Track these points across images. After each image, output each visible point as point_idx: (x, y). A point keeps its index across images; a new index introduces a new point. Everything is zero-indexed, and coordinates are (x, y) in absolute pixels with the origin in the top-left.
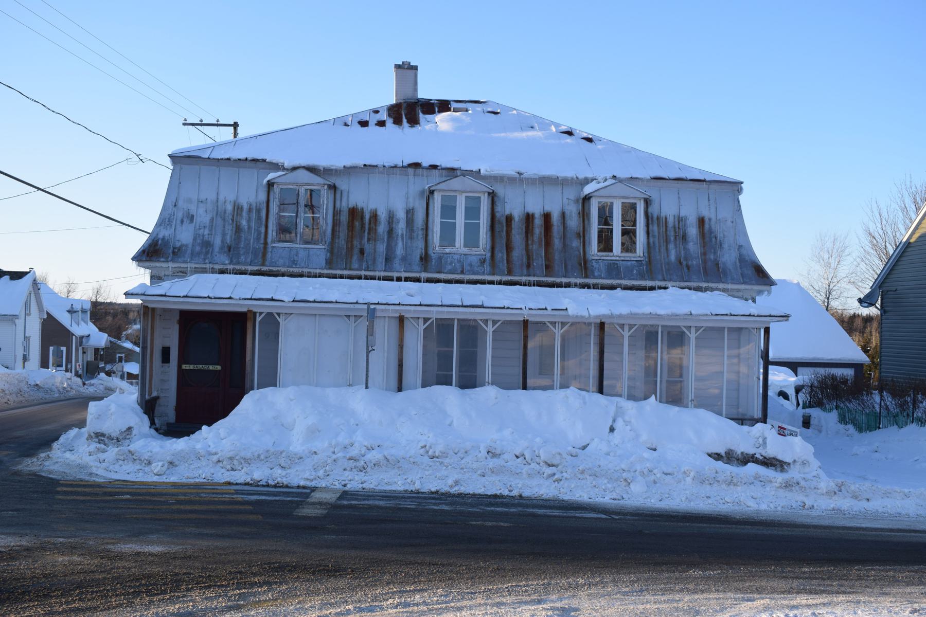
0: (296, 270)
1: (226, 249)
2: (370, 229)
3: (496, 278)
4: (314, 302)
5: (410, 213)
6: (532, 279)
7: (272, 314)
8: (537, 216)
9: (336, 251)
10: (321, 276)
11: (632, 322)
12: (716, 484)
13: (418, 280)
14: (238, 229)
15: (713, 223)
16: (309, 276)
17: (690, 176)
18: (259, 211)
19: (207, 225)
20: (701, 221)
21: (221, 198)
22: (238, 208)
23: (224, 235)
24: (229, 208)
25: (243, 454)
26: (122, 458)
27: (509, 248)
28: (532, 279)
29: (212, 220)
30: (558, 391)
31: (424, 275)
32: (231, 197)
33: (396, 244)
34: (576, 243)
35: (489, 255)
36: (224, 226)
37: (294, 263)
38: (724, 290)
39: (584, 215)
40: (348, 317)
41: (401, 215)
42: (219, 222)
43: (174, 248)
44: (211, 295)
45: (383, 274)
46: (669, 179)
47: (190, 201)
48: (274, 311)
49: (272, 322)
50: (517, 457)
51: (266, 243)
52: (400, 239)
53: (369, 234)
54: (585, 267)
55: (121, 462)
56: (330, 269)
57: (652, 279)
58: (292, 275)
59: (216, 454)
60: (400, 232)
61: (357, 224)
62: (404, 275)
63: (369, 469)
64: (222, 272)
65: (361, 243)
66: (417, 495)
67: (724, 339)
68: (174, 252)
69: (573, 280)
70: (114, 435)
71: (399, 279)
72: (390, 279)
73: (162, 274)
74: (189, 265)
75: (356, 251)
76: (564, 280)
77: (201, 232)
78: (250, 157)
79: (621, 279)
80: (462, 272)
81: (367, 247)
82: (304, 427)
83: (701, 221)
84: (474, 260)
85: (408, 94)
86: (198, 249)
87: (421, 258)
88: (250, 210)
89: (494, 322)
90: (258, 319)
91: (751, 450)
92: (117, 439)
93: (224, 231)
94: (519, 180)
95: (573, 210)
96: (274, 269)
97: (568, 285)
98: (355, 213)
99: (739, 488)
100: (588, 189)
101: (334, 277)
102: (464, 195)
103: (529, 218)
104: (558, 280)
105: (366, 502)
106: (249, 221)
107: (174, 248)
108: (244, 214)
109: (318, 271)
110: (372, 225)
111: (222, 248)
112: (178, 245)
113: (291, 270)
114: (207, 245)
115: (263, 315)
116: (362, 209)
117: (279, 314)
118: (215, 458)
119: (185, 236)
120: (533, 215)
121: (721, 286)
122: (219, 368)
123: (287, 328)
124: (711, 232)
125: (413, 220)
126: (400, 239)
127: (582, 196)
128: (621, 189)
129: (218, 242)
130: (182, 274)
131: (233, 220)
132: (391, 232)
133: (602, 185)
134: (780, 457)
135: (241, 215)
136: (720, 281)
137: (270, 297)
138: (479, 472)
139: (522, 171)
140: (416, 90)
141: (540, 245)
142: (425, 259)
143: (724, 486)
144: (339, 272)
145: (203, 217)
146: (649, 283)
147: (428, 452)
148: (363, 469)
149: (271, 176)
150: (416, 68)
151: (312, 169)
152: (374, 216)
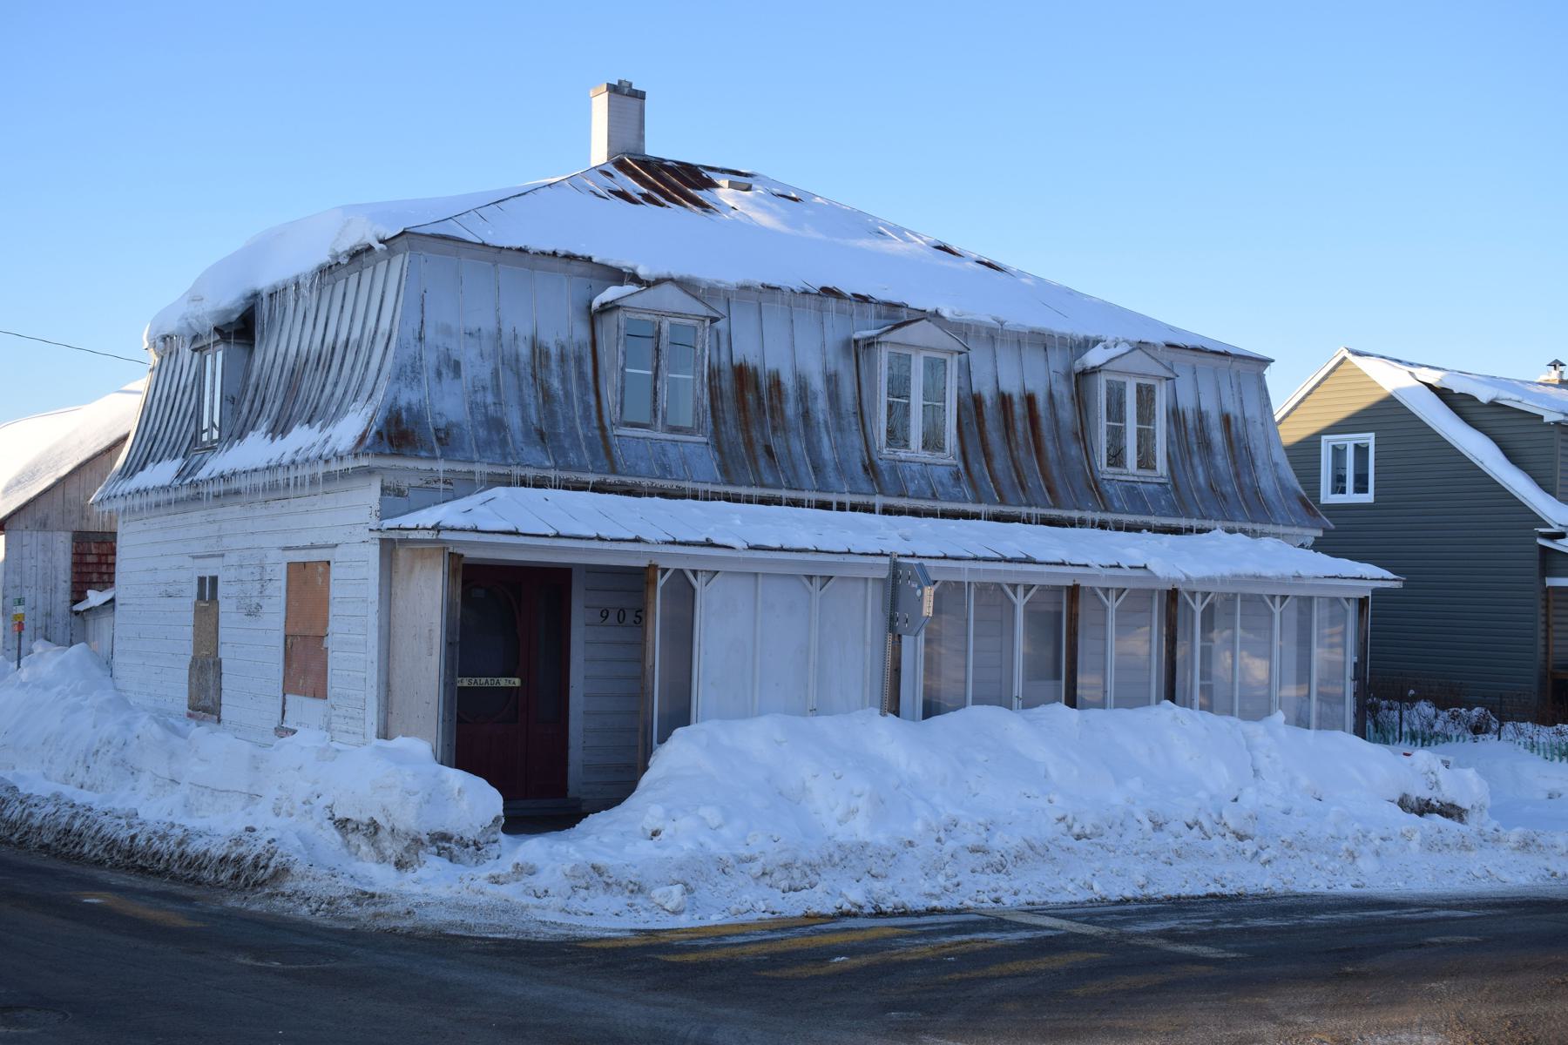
0: (667, 484)
1: (537, 438)
2: (772, 409)
3: (982, 508)
4: (782, 549)
5: (832, 380)
6: (1034, 511)
7: (682, 571)
8: (1016, 399)
9: (726, 448)
10: (715, 497)
11: (1122, 586)
12: (1446, 851)
13: (869, 509)
14: (547, 396)
15: (1240, 424)
16: (695, 497)
17: (1189, 344)
18: (579, 360)
19: (489, 383)
20: (1226, 420)
21: (507, 330)
22: (539, 353)
23: (523, 406)
24: (524, 350)
25: (804, 855)
26: (583, 883)
27: (988, 456)
28: (1034, 511)
29: (495, 374)
30: (1197, 713)
31: (879, 501)
32: (525, 330)
33: (820, 440)
34: (1074, 451)
35: (961, 466)
36: (521, 390)
37: (666, 471)
38: (1276, 536)
39: (1081, 401)
40: (810, 578)
41: (817, 384)
42: (507, 378)
43: (437, 430)
44: (603, 534)
45: (814, 496)
46: (1186, 348)
47: (447, 331)
48: (686, 566)
49: (683, 589)
50: (1191, 828)
51: (602, 428)
52: (823, 430)
53: (772, 418)
54: (1096, 492)
55: (583, 893)
56: (730, 483)
57: (1189, 516)
58: (665, 494)
59: (751, 859)
60: (821, 417)
61: (750, 397)
62: (848, 499)
63: (1009, 866)
64: (539, 484)
65: (763, 435)
66: (1092, 912)
67: (1234, 614)
68: (439, 439)
69: (1088, 515)
70: (469, 836)
71: (841, 507)
72: (825, 506)
73: (404, 485)
74: (477, 468)
75: (759, 450)
76: (1076, 514)
77: (479, 397)
78: (562, 250)
79: (1149, 514)
80: (934, 497)
81: (777, 444)
82: (774, 796)
83: (1226, 420)
84: (943, 474)
85: (631, 144)
86: (482, 433)
87: (865, 469)
88: (563, 358)
89: (1028, 588)
90: (661, 582)
91: (1426, 794)
92: (475, 843)
93: (521, 398)
94: (993, 336)
95: (1063, 390)
96: (629, 480)
97: (1082, 523)
98: (743, 375)
99: (1472, 854)
100: (1094, 357)
101: (736, 499)
102: (924, 353)
103: (1005, 401)
104: (1065, 514)
105: (982, 936)
106: (564, 380)
107: (437, 430)
108: (554, 365)
109: (710, 488)
110: (775, 401)
111: (527, 434)
112: (442, 423)
113: (659, 483)
114: (496, 425)
115: (668, 574)
116: (755, 369)
117: (695, 572)
118: (756, 868)
119: (448, 404)
120: (1010, 397)
121: (1270, 528)
122: (517, 682)
123: (708, 597)
124: (1240, 441)
125: (837, 396)
126: (823, 430)
127: (1078, 367)
128: (1140, 362)
129: (514, 419)
130: (455, 487)
131: (534, 377)
132: (806, 415)
133: (1113, 352)
134: (1459, 803)
135: (547, 367)
136: (1267, 521)
137: (702, 539)
138: (1163, 857)
139: (1002, 318)
140: (641, 137)
141: (1029, 453)
142: (870, 468)
143: (1455, 853)
144: (743, 491)
145: (477, 368)
146: (1183, 522)
147: (1070, 828)
148: (1000, 868)
149: (611, 293)
150: (641, 96)
151: (686, 285)
152: (776, 383)
